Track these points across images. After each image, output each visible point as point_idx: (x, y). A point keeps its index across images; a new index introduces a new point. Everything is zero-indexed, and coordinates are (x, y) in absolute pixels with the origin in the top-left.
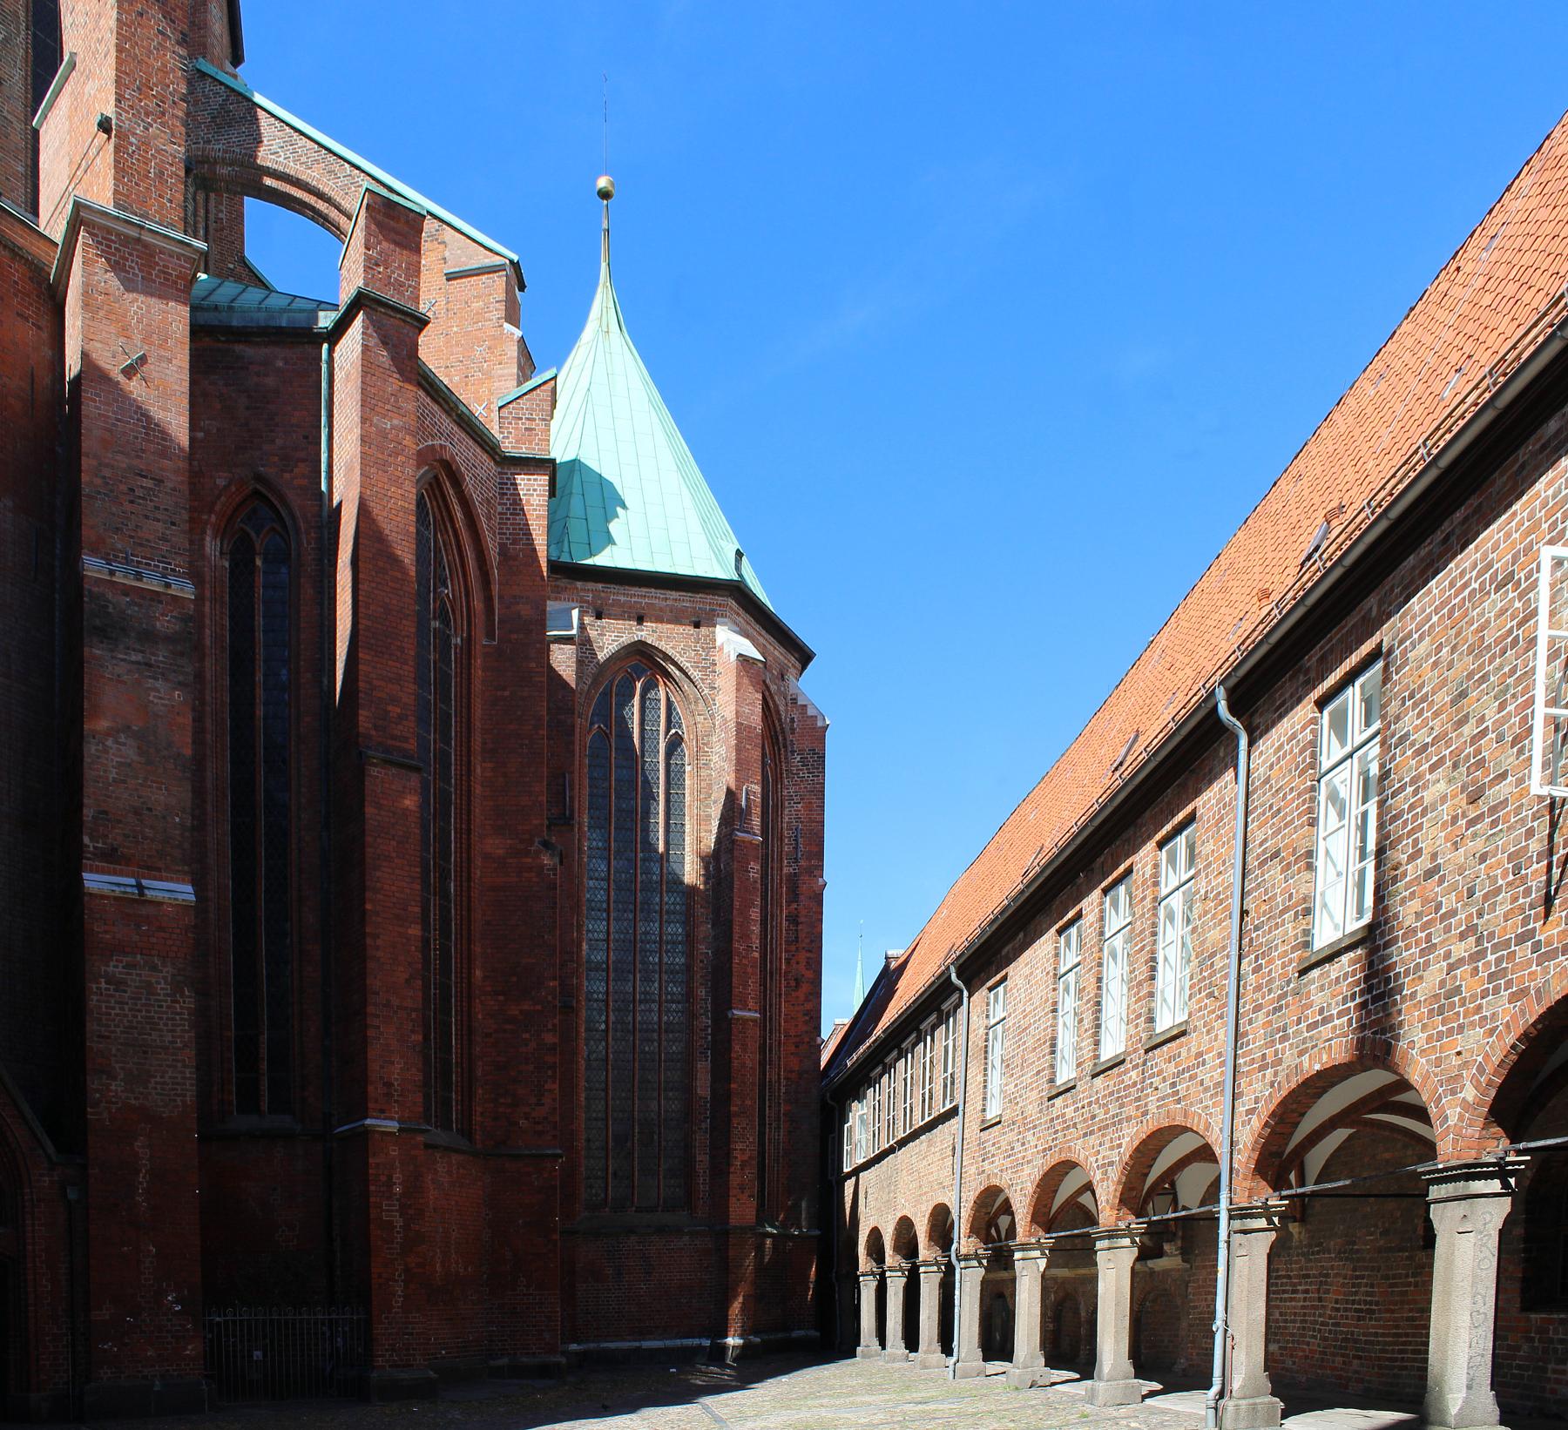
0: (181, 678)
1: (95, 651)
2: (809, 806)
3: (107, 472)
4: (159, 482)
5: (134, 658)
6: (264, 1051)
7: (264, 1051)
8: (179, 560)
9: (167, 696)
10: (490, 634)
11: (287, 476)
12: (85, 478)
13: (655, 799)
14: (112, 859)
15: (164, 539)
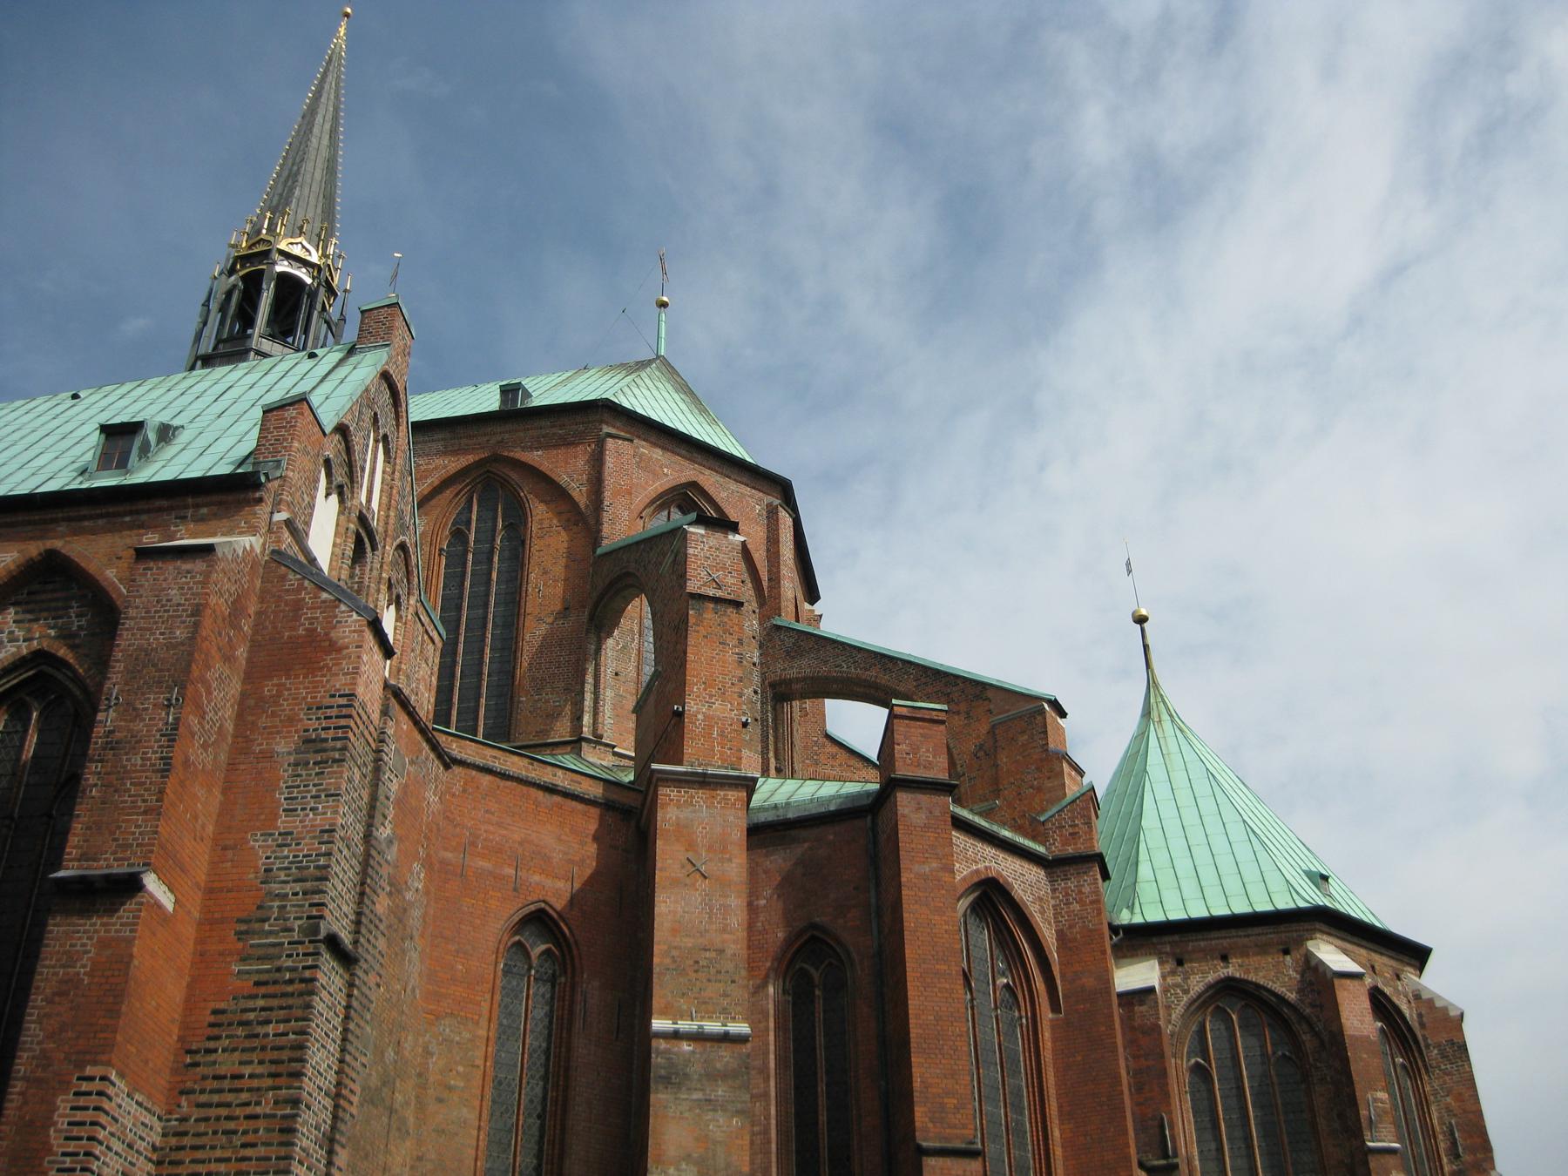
0: (739, 1106)
1: (659, 1098)
2: (1459, 1098)
3: (675, 953)
4: (721, 951)
5: (695, 1096)
6: (825, 1153)
7: (825, 1153)
8: (739, 1009)
9: (726, 1127)
10: (1055, 1007)
11: (841, 921)
12: (656, 960)
13: (1262, 1125)
14: (664, 1014)
15: (725, 995)
